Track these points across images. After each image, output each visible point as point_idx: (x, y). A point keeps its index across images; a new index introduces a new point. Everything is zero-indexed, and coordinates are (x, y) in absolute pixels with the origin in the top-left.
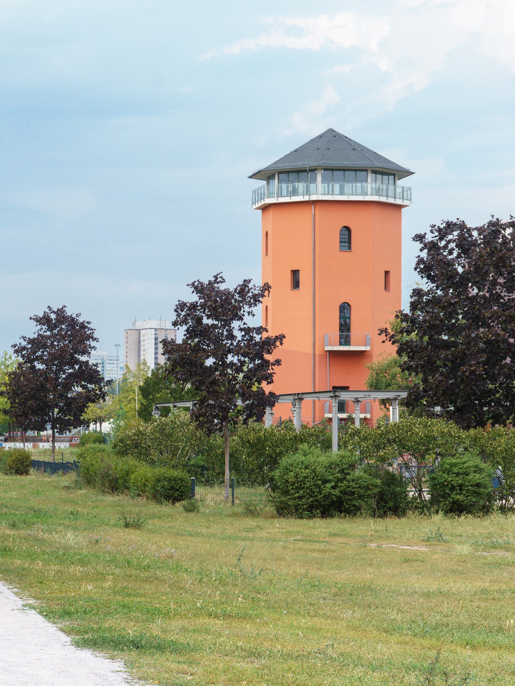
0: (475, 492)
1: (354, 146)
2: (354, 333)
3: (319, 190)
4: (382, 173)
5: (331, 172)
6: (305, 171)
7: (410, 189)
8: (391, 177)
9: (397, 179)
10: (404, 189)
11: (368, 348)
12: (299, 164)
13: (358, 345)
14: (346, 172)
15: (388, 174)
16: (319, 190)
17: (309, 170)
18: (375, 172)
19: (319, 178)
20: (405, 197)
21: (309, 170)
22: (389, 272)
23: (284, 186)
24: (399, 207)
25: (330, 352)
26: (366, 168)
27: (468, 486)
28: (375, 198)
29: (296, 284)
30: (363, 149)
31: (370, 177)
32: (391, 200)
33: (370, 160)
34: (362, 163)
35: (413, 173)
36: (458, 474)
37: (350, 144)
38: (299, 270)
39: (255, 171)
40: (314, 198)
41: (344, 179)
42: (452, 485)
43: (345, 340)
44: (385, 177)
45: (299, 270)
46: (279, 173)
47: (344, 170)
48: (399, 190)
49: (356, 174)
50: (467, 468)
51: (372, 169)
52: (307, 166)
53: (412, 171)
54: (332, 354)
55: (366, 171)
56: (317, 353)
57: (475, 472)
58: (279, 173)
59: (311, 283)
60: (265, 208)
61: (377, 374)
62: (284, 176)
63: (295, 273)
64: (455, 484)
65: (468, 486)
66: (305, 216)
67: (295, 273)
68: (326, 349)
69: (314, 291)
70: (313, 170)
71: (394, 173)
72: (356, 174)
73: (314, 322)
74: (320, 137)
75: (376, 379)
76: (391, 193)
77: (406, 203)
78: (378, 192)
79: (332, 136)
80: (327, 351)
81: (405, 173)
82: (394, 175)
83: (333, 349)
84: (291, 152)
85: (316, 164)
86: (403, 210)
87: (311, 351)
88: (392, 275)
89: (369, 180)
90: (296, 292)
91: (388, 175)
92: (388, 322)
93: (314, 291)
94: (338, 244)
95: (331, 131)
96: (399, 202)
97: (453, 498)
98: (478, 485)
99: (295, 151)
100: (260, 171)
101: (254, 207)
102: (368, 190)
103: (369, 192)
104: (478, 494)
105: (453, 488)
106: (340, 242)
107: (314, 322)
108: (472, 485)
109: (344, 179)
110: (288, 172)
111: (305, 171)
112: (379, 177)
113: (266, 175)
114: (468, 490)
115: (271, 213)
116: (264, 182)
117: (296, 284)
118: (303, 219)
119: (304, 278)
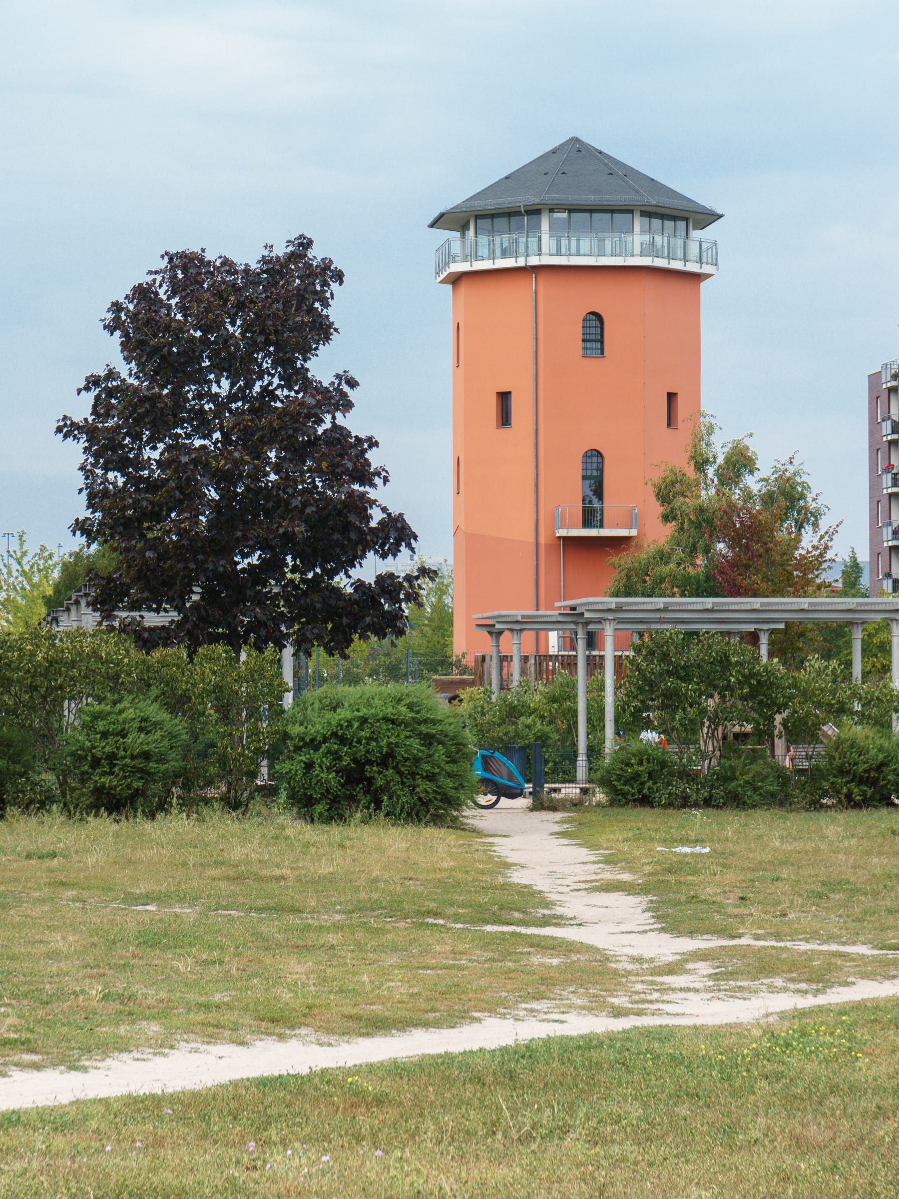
0: (141, 770)
1: (611, 168)
2: (612, 504)
3: (546, 247)
4: (663, 217)
5: (588, 215)
6: (518, 213)
7: (716, 244)
8: (682, 225)
9: (691, 227)
10: (704, 246)
11: (633, 533)
12: (508, 201)
13: (618, 526)
14: (615, 215)
15: (674, 218)
16: (546, 247)
17: (526, 212)
18: (648, 214)
19: (545, 225)
20: (704, 260)
21: (526, 212)
22: (676, 394)
23: (483, 240)
24: (697, 277)
25: (566, 539)
26: (631, 208)
27: (124, 758)
28: (646, 261)
29: (505, 419)
30: (629, 173)
31: (638, 223)
32: (677, 265)
33: (638, 192)
34: (621, 198)
35: (720, 216)
36: (105, 735)
37: (606, 165)
38: (510, 393)
39: (436, 214)
40: (534, 261)
41: (612, 229)
42: (93, 756)
43: (590, 517)
44: (669, 224)
45: (510, 393)
46: (477, 217)
47: (591, 210)
48: (694, 249)
49: (591, 217)
50: (124, 722)
51: (643, 209)
52: (522, 204)
53: (719, 212)
54: (569, 542)
55: (631, 212)
56: (542, 541)
57: (141, 729)
58: (477, 217)
59: (531, 418)
60: (456, 280)
61: (628, 577)
62: (485, 223)
63: (504, 397)
64: (99, 755)
65: (124, 758)
66: (519, 294)
67: (504, 397)
68: (558, 535)
69: (537, 430)
70: (534, 212)
71: (692, 217)
72: (591, 217)
73: (537, 485)
74: (554, 152)
75: (625, 586)
76: (680, 253)
77: (706, 269)
78: (650, 250)
79: (576, 149)
80: (559, 537)
81: (705, 216)
82: (687, 220)
83: (569, 535)
84: (500, 180)
85: (538, 200)
86: (704, 285)
87: (532, 539)
88: (681, 401)
89: (637, 228)
90: (505, 432)
91: (675, 221)
92: (650, 483)
93: (537, 430)
94: (581, 344)
95: (575, 140)
96: (692, 267)
97: (96, 782)
98: (146, 756)
99: (507, 178)
100: (442, 215)
101: (439, 279)
102: (636, 245)
103: (637, 250)
104: (145, 774)
105: (96, 763)
106: (584, 341)
107: (537, 485)
108: (133, 757)
109: (612, 229)
110: (492, 216)
111: (518, 213)
112: (656, 222)
113: (455, 220)
114: (125, 765)
115: (463, 288)
116: (458, 234)
117: (505, 419)
118: (516, 299)
119: (520, 407)
